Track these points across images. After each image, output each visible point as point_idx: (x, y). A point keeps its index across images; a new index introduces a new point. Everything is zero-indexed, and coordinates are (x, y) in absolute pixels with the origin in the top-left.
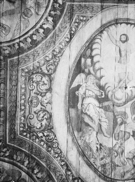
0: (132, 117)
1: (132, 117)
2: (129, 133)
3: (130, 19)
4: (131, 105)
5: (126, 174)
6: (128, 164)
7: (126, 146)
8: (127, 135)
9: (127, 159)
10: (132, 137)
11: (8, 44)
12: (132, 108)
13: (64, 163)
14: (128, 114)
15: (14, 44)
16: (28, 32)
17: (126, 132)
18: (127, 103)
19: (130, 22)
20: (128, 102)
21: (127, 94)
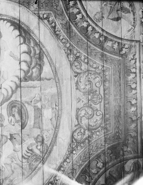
0: (8, 120)
1: (8, 120)
2: (6, 137)
3: (3, 14)
4: (8, 106)
5: (5, 180)
6: (6, 170)
7: (58, 70)
8: (4, 138)
9: (5, 164)
10: (9, 140)
11: (85, 15)
12: (8, 109)
13: (63, 41)
14: (4, 115)
15: (136, 69)
16: (139, 71)
17: (3, 136)
18: (3, 104)
19: (3, 17)
20: (4, 102)
21: (3, 94)
